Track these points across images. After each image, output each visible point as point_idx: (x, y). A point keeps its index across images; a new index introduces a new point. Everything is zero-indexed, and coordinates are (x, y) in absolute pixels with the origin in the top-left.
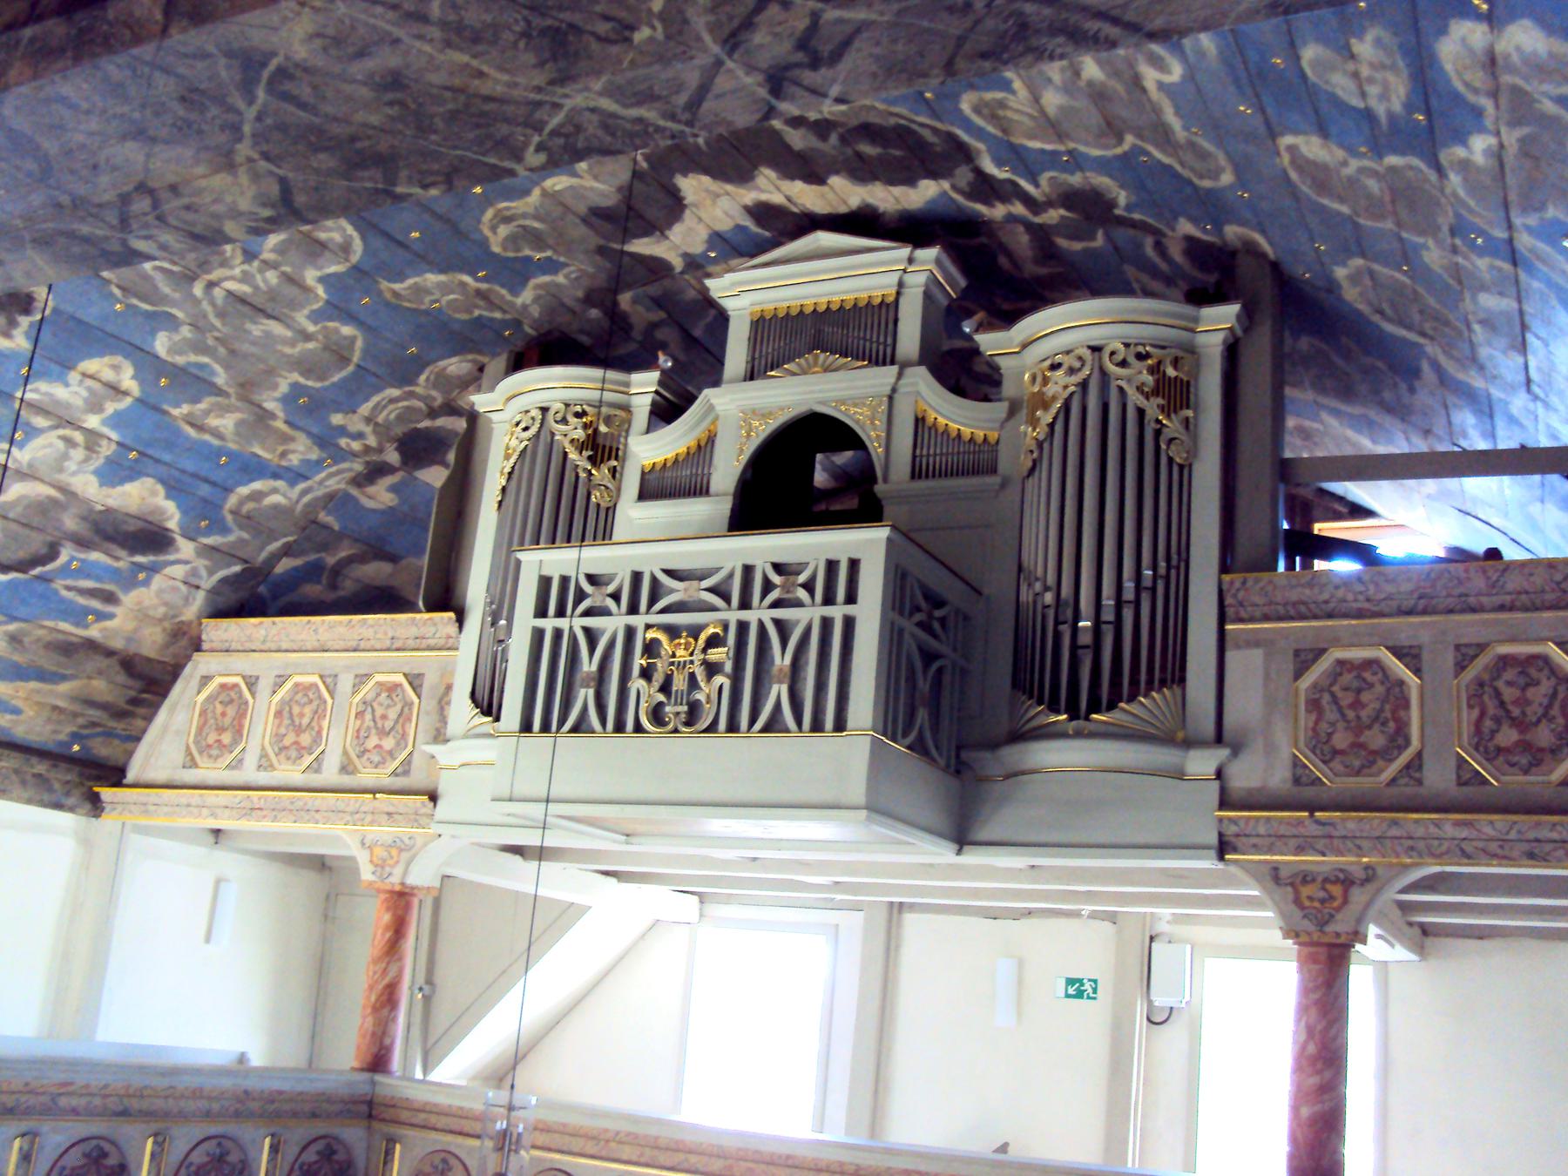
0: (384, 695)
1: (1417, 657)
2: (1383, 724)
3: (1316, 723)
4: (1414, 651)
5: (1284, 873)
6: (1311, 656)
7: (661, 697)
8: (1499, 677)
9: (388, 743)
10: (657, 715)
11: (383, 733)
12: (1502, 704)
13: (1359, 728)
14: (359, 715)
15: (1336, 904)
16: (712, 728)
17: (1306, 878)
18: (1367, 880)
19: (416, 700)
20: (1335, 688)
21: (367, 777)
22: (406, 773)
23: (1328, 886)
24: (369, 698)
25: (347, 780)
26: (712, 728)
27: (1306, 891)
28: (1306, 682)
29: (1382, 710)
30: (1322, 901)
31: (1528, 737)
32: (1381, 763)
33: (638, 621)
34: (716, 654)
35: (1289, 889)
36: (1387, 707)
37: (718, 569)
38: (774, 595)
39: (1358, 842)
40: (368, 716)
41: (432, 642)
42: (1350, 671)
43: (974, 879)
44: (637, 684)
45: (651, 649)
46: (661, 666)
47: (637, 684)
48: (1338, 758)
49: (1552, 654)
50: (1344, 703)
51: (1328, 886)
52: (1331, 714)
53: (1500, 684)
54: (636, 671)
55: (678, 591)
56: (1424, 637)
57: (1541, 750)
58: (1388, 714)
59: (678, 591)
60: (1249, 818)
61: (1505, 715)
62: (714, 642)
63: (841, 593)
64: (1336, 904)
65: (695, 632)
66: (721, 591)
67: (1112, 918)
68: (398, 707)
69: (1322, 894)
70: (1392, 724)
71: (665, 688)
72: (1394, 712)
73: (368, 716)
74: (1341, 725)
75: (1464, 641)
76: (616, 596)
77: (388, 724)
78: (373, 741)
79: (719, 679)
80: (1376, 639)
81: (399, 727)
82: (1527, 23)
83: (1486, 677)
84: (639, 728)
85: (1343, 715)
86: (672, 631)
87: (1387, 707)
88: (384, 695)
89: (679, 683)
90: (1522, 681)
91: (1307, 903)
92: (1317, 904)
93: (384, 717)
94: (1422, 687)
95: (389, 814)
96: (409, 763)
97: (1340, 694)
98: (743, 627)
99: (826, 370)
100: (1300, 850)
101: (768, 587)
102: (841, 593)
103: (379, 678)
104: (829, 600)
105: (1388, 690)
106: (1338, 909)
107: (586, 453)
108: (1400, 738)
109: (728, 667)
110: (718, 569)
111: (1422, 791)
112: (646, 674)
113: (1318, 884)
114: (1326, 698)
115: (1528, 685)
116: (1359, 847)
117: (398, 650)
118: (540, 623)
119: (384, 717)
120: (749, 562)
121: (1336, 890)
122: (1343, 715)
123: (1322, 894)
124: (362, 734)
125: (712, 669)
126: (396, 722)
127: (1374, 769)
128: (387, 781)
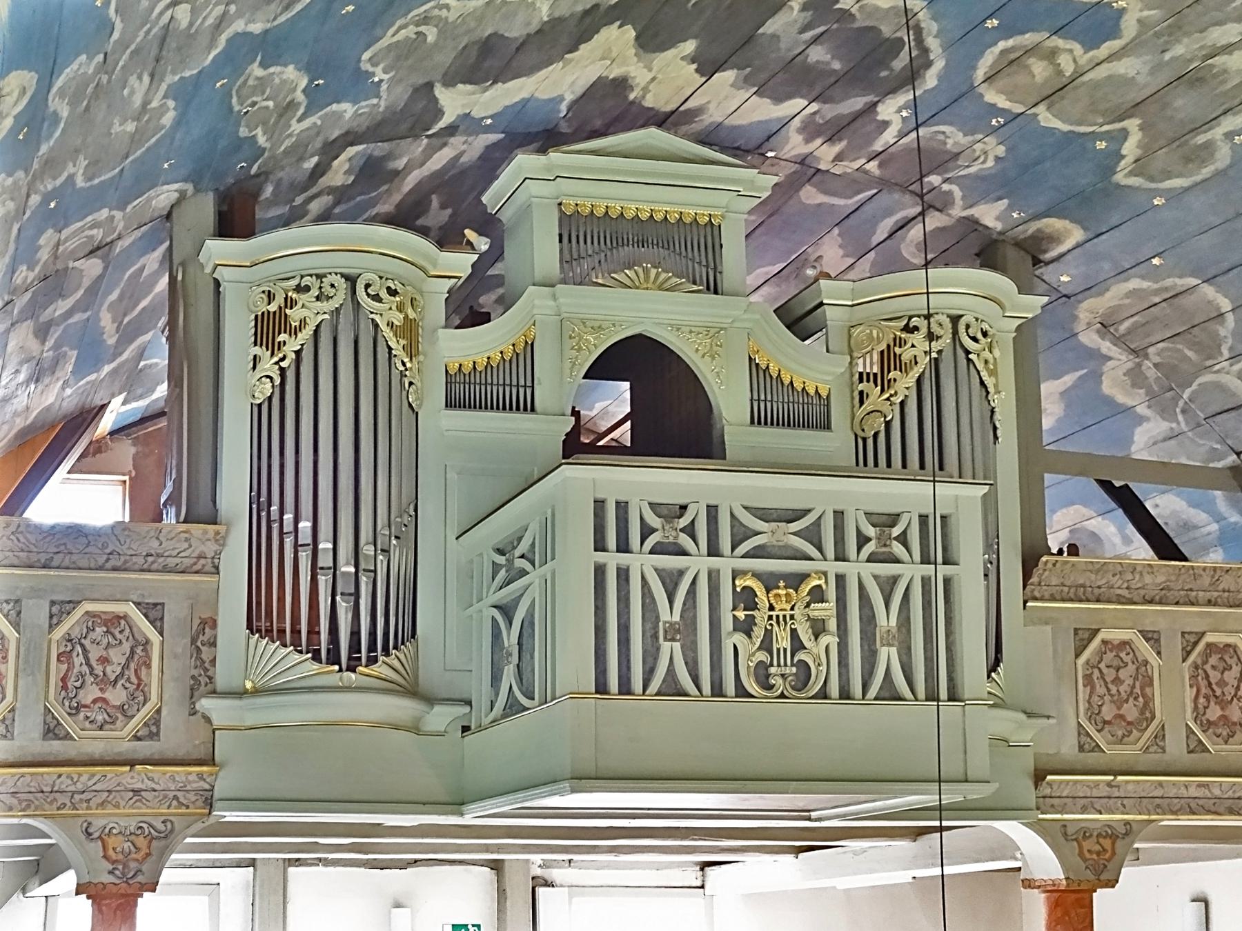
0: (100, 630)
1: (1158, 641)
2: (1136, 699)
3: (1090, 696)
4: (1155, 636)
5: (1070, 830)
6: (1086, 635)
7: (762, 656)
8: (1205, 662)
9: (117, 696)
10: (762, 675)
11: (104, 682)
12: (1210, 684)
13: (1119, 704)
14: (65, 657)
15: (1107, 856)
16: (823, 694)
17: (1085, 833)
18: (1126, 834)
19: (154, 637)
20: (1102, 666)
21: (90, 742)
22: (154, 736)
23: (1101, 840)
24: (76, 633)
25: (56, 748)
26: (823, 694)
27: (1087, 845)
28: (59, 633)
29: (1133, 687)
30: (1098, 854)
31: (1227, 713)
32: (1135, 733)
33: (725, 565)
34: (818, 610)
35: (1075, 843)
36: (1138, 684)
37: (807, 512)
38: (870, 548)
39: (1125, 801)
40: (78, 660)
41: (172, 562)
42: (1111, 651)
43: (683, 838)
44: (732, 639)
45: (746, 599)
46: (761, 616)
47: (732, 639)
48: (1107, 728)
49: (130, 614)
50: (1213, 681)
51: (1101, 840)
52: (1101, 690)
53: (1208, 667)
54: (727, 624)
55: (767, 534)
56: (1161, 625)
57: (1235, 724)
58: (1137, 690)
59: (767, 534)
60: (1061, 782)
61: (1212, 696)
62: (818, 595)
63: (612, 542)
64: (1107, 856)
65: (795, 581)
66: (813, 535)
67: (252, 863)
68: (126, 647)
69: (1098, 848)
70: (1141, 699)
71: (766, 645)
72: (1142, 689)
73: (78, 660)
74: (1107, 698)
75: (1188, 630)
76: (690, 531)
77: (113, 671)
78: (91, 693)
79: (825, 640)
80: (1130, 624)
81: (130, 673)
82: (258, 32)
83: (1199, 662)
84: (742, 692)
85: (1109, 690)
86: (770, 582)
87: (1138, 684)
88: (100, 630)
89: (782, 641)
90: (1221, 665)
91: (1088, 855)
92: (1095, 856)
93: (104, 660)
94: (18, 641)
95: (136, 792)
96: (157, 723)
97: (1105, 671)
98: (840, 579)
99: (660, 288)
100: (1084, 810)
101: (863, 540)
102: (612, 542)
103: (1210, 638)
104: (713, 551)
105: (1137, 669)
106: (1108, 860)
107: (402, 342)
108: (140, 691)
109: (832, 625)
110: (807, 512)
111: (1166, 757)
112: (746, 628)
113: (1094, 839)
114: (1096, 673)
115: (1225, 669)
116: (1124, 806)
117: (115, 569)
118: (601, 557)
119: (104, 660)
120: (622, 498)
121: (1107, 843)
122: (1109, 690)
123: (1098, 848)
124: (71, 683)
125: (818, 629)
126: (126, 666)
127: (1132, 738)
128: (126, 747)
